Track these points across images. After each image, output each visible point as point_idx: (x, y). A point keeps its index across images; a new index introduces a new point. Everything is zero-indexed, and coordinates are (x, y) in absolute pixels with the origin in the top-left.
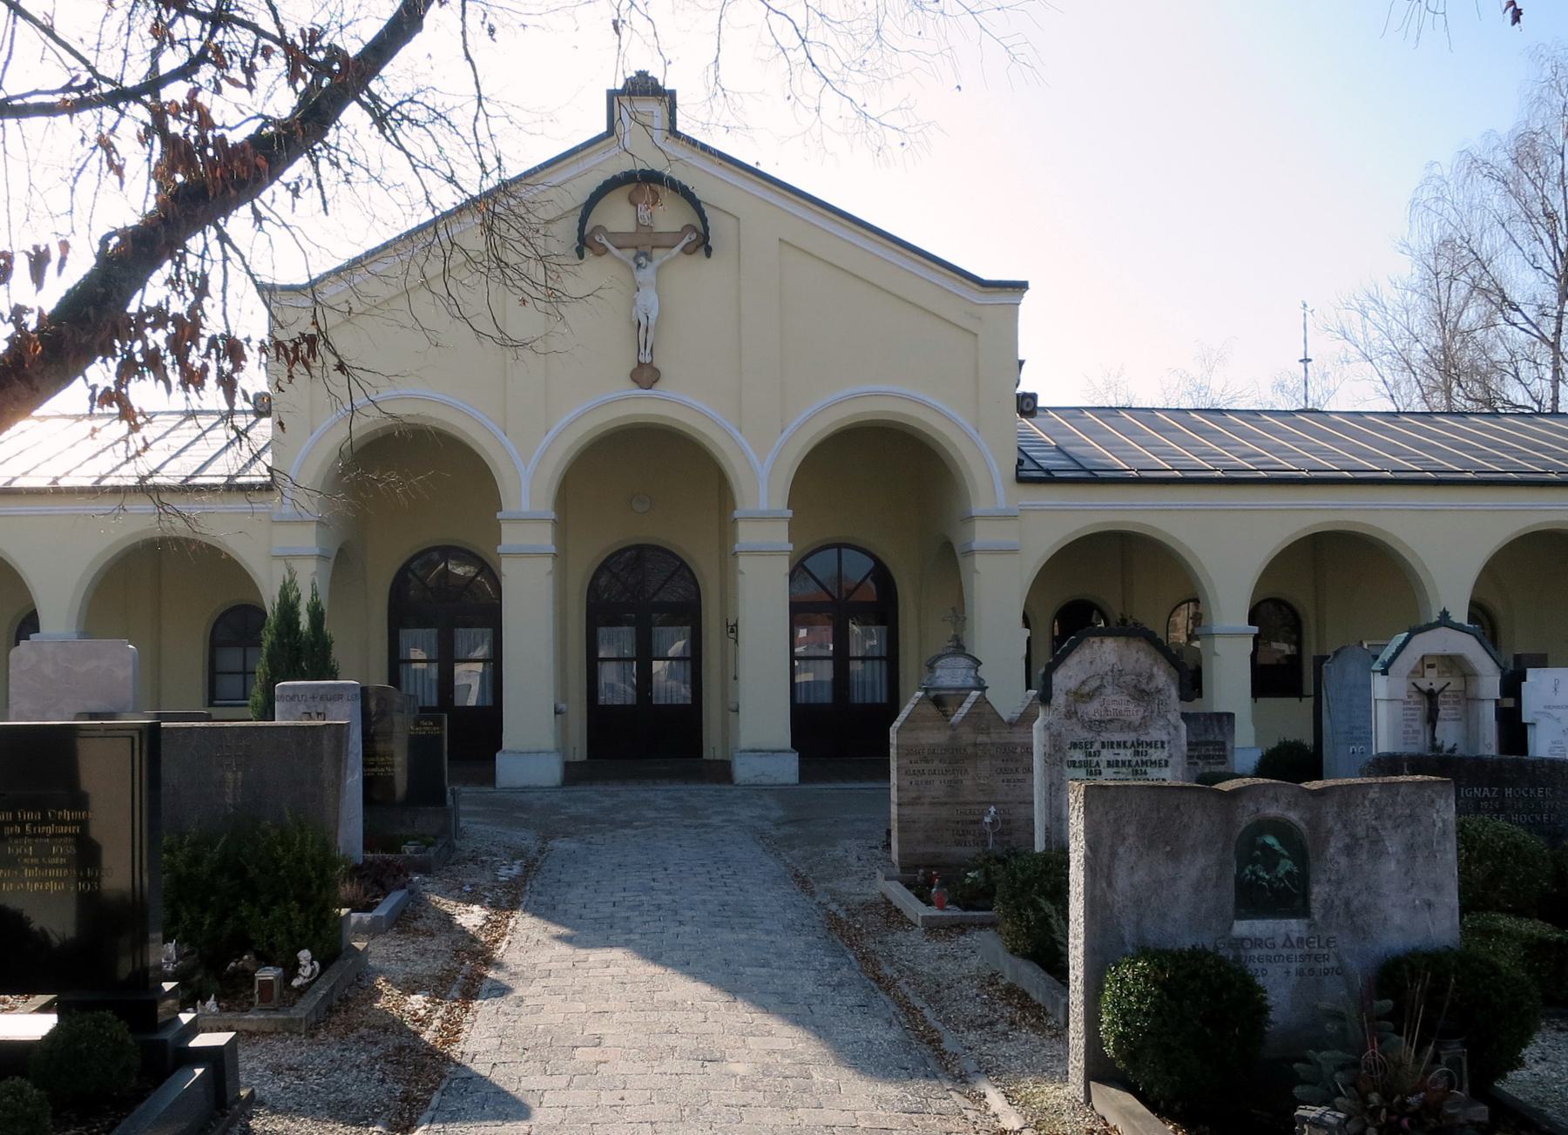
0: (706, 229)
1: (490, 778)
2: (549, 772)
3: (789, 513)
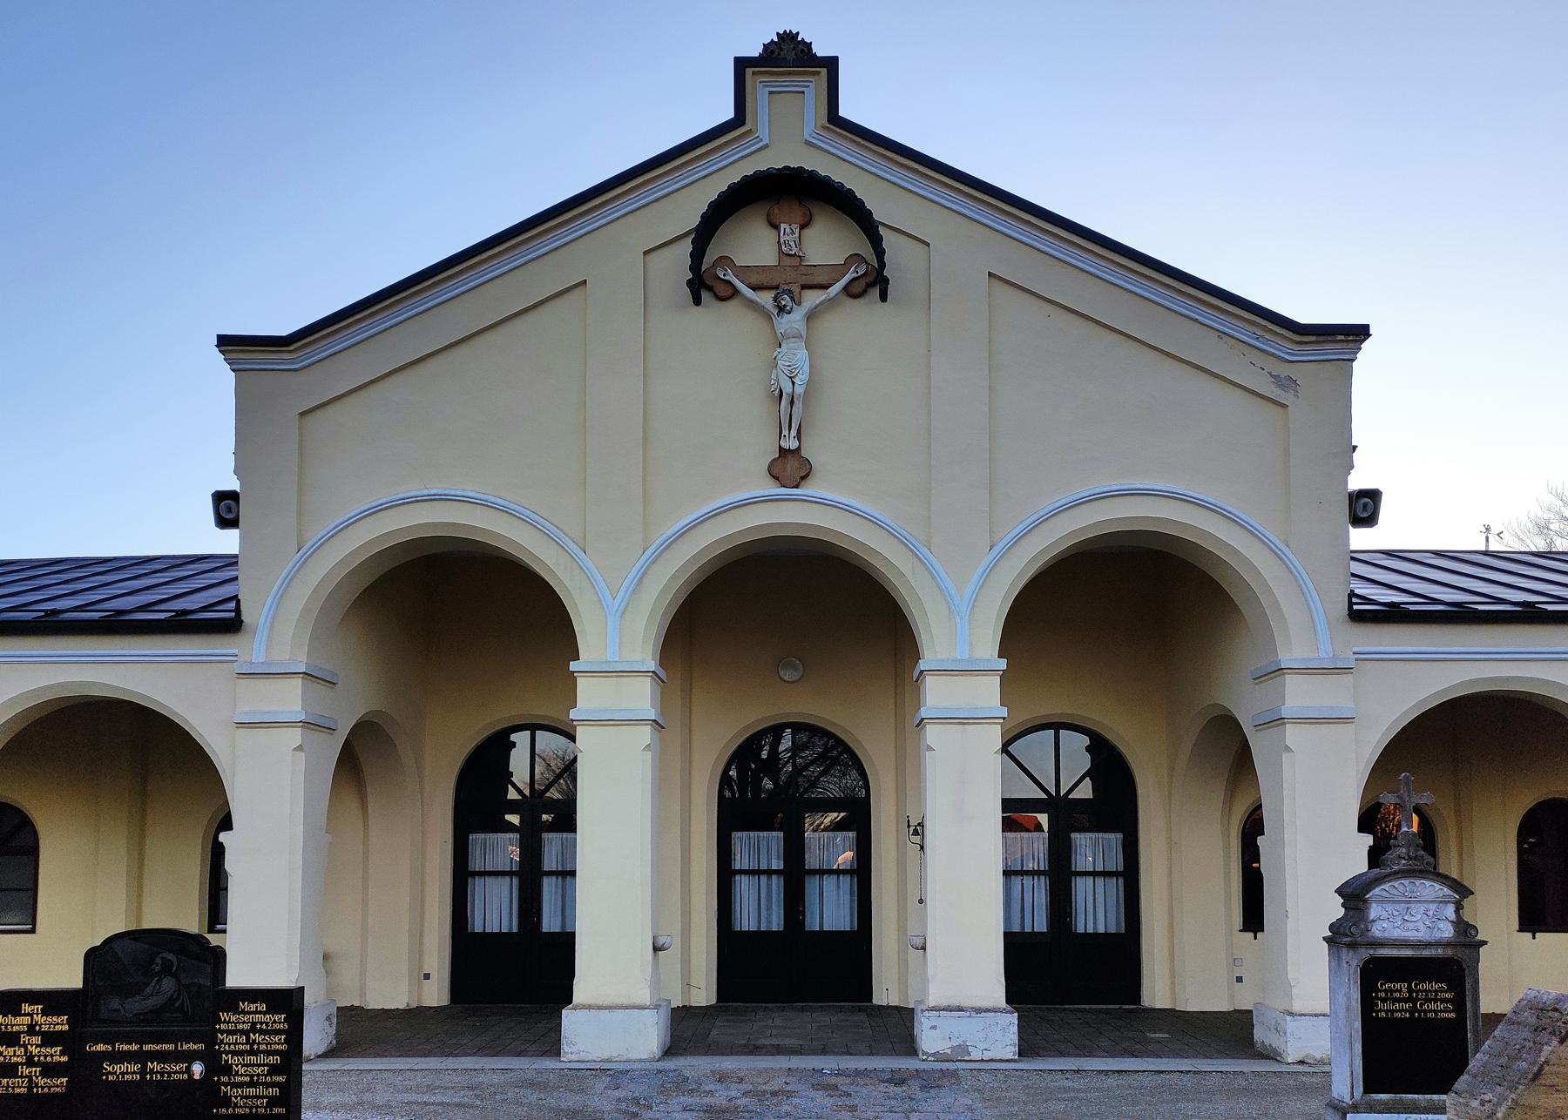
0: (882, 265)
1: (551, 1045)
2: (643, 1039)
3: (1002, 664)
